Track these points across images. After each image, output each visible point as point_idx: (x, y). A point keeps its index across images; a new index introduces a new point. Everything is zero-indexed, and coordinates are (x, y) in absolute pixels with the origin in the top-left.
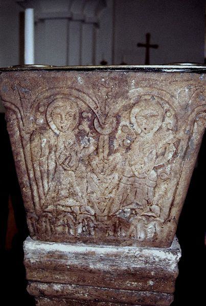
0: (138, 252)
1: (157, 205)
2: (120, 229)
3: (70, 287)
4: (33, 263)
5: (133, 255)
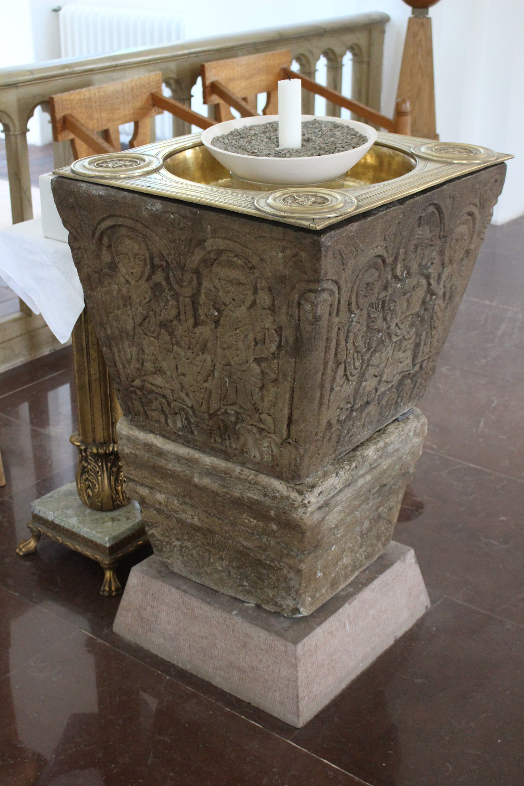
0: (251, 477)
1: (269, 415)
2: (229, 436)
4: (127, 454)
5: (246, 478)
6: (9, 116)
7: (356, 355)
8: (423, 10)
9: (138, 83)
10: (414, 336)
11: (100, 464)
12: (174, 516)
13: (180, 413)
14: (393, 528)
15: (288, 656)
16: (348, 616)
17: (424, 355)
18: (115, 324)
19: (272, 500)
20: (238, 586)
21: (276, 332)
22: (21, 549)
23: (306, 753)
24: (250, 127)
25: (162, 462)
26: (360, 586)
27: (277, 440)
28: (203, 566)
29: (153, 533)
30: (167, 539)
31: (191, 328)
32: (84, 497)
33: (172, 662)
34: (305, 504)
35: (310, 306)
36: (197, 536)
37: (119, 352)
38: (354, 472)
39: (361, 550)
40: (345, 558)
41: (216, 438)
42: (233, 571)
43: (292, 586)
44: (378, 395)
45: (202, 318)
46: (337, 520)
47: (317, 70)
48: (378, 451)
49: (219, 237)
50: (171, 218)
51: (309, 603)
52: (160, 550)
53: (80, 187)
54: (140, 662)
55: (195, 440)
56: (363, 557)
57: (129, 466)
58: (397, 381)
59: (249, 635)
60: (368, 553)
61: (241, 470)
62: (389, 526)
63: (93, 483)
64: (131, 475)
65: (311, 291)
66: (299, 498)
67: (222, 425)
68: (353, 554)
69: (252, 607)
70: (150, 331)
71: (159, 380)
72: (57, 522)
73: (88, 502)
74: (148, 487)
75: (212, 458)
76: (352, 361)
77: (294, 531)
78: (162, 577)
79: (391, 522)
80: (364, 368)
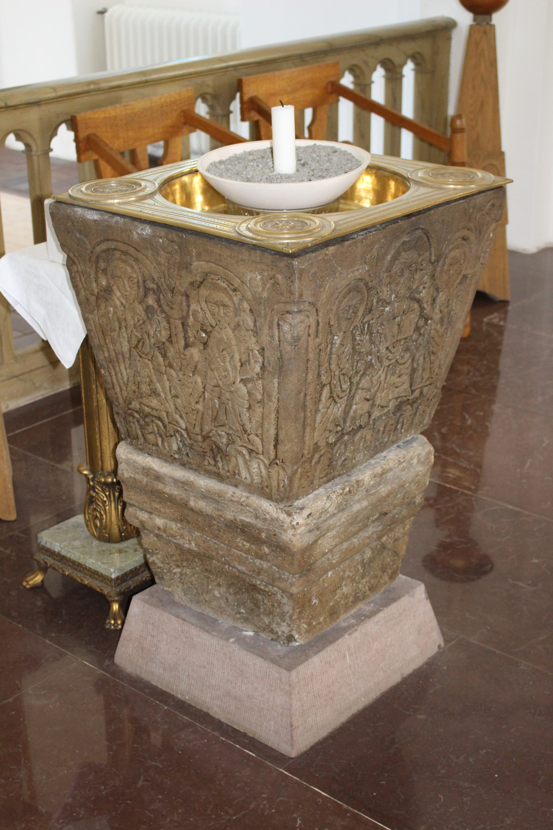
3: (174, 526)
4: (127, 478)
6: (31, 136)
7: (342, 377)
8: (486, 17)
9: (168, 100)
10: (410, 361)
11: (107, 493)
12: (173, 542)
13: (175, 435)
14: (401, 560)
15: (282, 683)
16: (349, 647)
17: (424, 381)
18: (111, 346)
19: (263, 522)
20: (236, 613)
21: (259, 353)
22: (27, 582)
23: (297, 781)
24: (249, 152)
25: (160, 486)
26: (363, 618)
27: (265, 461)
28: (202, 593)
29: (154, 561)
30: (167, 567)
31: (182, 350)
32: (91, 528)
33: (171, 693)
34: (293, 525)
35: (288, 327)
36: (195, 562)
37: (116, 375)
38: (347, 497)
39: (364, 580)
40: (344, 587)
41: (210, 460)
42: (230, 598)
43: (286, 612)
44: (373, 420)
45: (192, 339)
46: (332, 545)
47: (373, 82)
48: (375, 477)
49: (203, 261)
50: (160, 242)
51: (305, 630)
52: (162, 578)
53: (76, 211)
54: (139, 692)
55: (190, 463)
56: (367, 588)
57: (129, 491)
58: (394, 406)
59: (245, 662)
60: (372, 585)
61: (234, 493)
62: (396, 558)
63: (100, 513)
64: (131, 499)
65: (288, 312)
66: (288, 520)
67: (214, 447)
68: (354, 584)
69: (250, 636)
70: (144, 353)
71: (154, 402)
72: (63, 553)
73: (95, 533)
74: (148, 512)
75: (206, 481)
76: (338, 383)
77: (284, 554)
78: (163, 605)
79: (398, 554)
80: (353, 391)
